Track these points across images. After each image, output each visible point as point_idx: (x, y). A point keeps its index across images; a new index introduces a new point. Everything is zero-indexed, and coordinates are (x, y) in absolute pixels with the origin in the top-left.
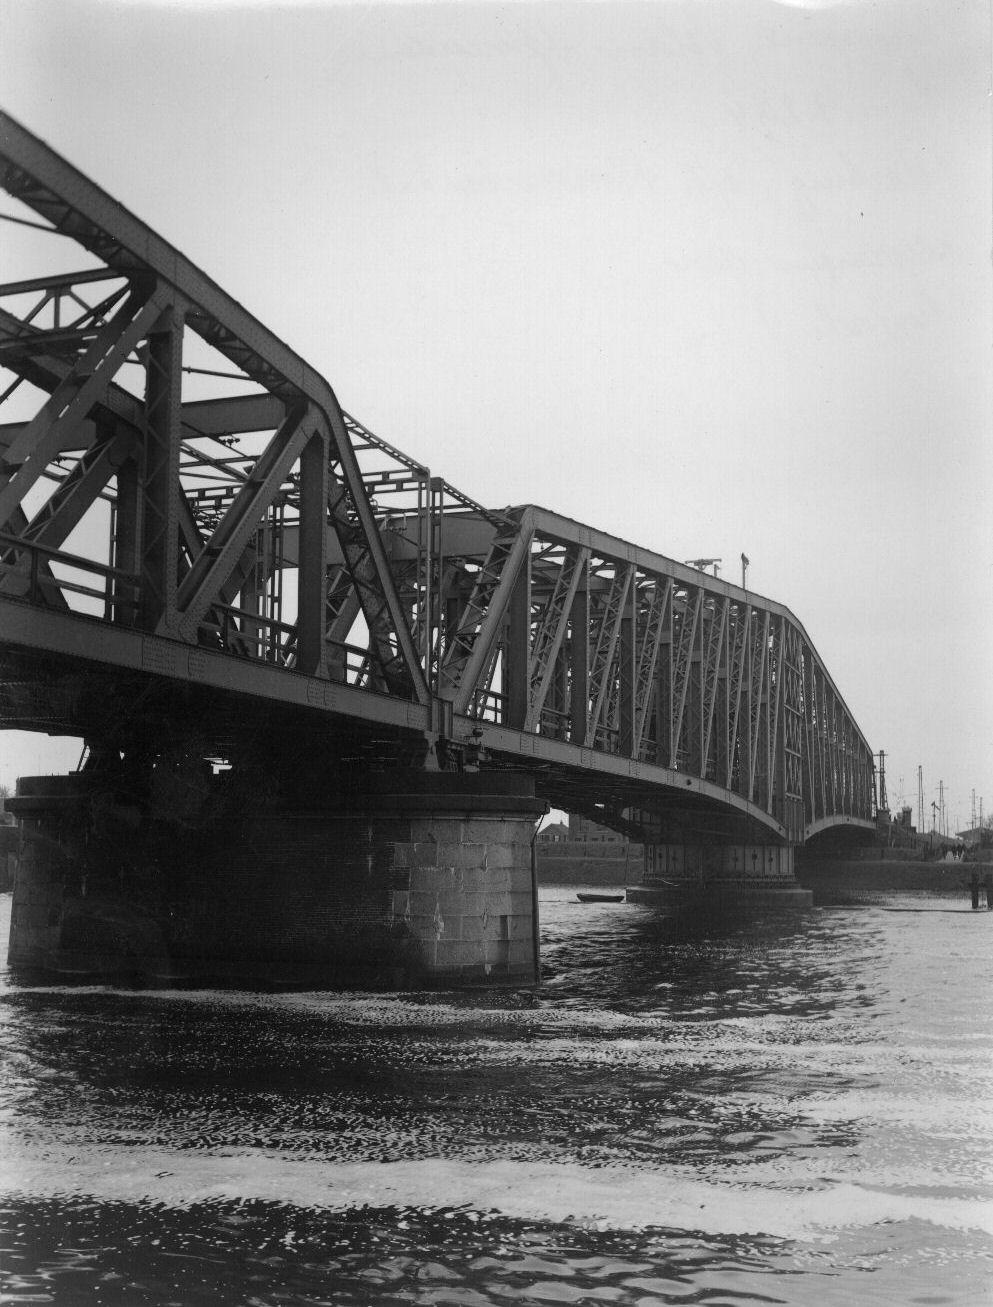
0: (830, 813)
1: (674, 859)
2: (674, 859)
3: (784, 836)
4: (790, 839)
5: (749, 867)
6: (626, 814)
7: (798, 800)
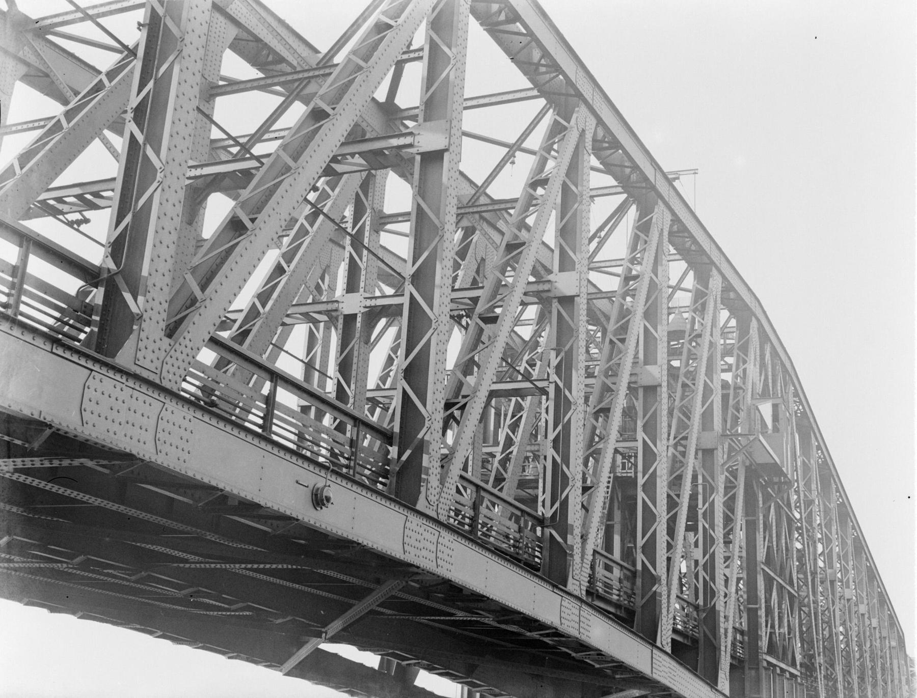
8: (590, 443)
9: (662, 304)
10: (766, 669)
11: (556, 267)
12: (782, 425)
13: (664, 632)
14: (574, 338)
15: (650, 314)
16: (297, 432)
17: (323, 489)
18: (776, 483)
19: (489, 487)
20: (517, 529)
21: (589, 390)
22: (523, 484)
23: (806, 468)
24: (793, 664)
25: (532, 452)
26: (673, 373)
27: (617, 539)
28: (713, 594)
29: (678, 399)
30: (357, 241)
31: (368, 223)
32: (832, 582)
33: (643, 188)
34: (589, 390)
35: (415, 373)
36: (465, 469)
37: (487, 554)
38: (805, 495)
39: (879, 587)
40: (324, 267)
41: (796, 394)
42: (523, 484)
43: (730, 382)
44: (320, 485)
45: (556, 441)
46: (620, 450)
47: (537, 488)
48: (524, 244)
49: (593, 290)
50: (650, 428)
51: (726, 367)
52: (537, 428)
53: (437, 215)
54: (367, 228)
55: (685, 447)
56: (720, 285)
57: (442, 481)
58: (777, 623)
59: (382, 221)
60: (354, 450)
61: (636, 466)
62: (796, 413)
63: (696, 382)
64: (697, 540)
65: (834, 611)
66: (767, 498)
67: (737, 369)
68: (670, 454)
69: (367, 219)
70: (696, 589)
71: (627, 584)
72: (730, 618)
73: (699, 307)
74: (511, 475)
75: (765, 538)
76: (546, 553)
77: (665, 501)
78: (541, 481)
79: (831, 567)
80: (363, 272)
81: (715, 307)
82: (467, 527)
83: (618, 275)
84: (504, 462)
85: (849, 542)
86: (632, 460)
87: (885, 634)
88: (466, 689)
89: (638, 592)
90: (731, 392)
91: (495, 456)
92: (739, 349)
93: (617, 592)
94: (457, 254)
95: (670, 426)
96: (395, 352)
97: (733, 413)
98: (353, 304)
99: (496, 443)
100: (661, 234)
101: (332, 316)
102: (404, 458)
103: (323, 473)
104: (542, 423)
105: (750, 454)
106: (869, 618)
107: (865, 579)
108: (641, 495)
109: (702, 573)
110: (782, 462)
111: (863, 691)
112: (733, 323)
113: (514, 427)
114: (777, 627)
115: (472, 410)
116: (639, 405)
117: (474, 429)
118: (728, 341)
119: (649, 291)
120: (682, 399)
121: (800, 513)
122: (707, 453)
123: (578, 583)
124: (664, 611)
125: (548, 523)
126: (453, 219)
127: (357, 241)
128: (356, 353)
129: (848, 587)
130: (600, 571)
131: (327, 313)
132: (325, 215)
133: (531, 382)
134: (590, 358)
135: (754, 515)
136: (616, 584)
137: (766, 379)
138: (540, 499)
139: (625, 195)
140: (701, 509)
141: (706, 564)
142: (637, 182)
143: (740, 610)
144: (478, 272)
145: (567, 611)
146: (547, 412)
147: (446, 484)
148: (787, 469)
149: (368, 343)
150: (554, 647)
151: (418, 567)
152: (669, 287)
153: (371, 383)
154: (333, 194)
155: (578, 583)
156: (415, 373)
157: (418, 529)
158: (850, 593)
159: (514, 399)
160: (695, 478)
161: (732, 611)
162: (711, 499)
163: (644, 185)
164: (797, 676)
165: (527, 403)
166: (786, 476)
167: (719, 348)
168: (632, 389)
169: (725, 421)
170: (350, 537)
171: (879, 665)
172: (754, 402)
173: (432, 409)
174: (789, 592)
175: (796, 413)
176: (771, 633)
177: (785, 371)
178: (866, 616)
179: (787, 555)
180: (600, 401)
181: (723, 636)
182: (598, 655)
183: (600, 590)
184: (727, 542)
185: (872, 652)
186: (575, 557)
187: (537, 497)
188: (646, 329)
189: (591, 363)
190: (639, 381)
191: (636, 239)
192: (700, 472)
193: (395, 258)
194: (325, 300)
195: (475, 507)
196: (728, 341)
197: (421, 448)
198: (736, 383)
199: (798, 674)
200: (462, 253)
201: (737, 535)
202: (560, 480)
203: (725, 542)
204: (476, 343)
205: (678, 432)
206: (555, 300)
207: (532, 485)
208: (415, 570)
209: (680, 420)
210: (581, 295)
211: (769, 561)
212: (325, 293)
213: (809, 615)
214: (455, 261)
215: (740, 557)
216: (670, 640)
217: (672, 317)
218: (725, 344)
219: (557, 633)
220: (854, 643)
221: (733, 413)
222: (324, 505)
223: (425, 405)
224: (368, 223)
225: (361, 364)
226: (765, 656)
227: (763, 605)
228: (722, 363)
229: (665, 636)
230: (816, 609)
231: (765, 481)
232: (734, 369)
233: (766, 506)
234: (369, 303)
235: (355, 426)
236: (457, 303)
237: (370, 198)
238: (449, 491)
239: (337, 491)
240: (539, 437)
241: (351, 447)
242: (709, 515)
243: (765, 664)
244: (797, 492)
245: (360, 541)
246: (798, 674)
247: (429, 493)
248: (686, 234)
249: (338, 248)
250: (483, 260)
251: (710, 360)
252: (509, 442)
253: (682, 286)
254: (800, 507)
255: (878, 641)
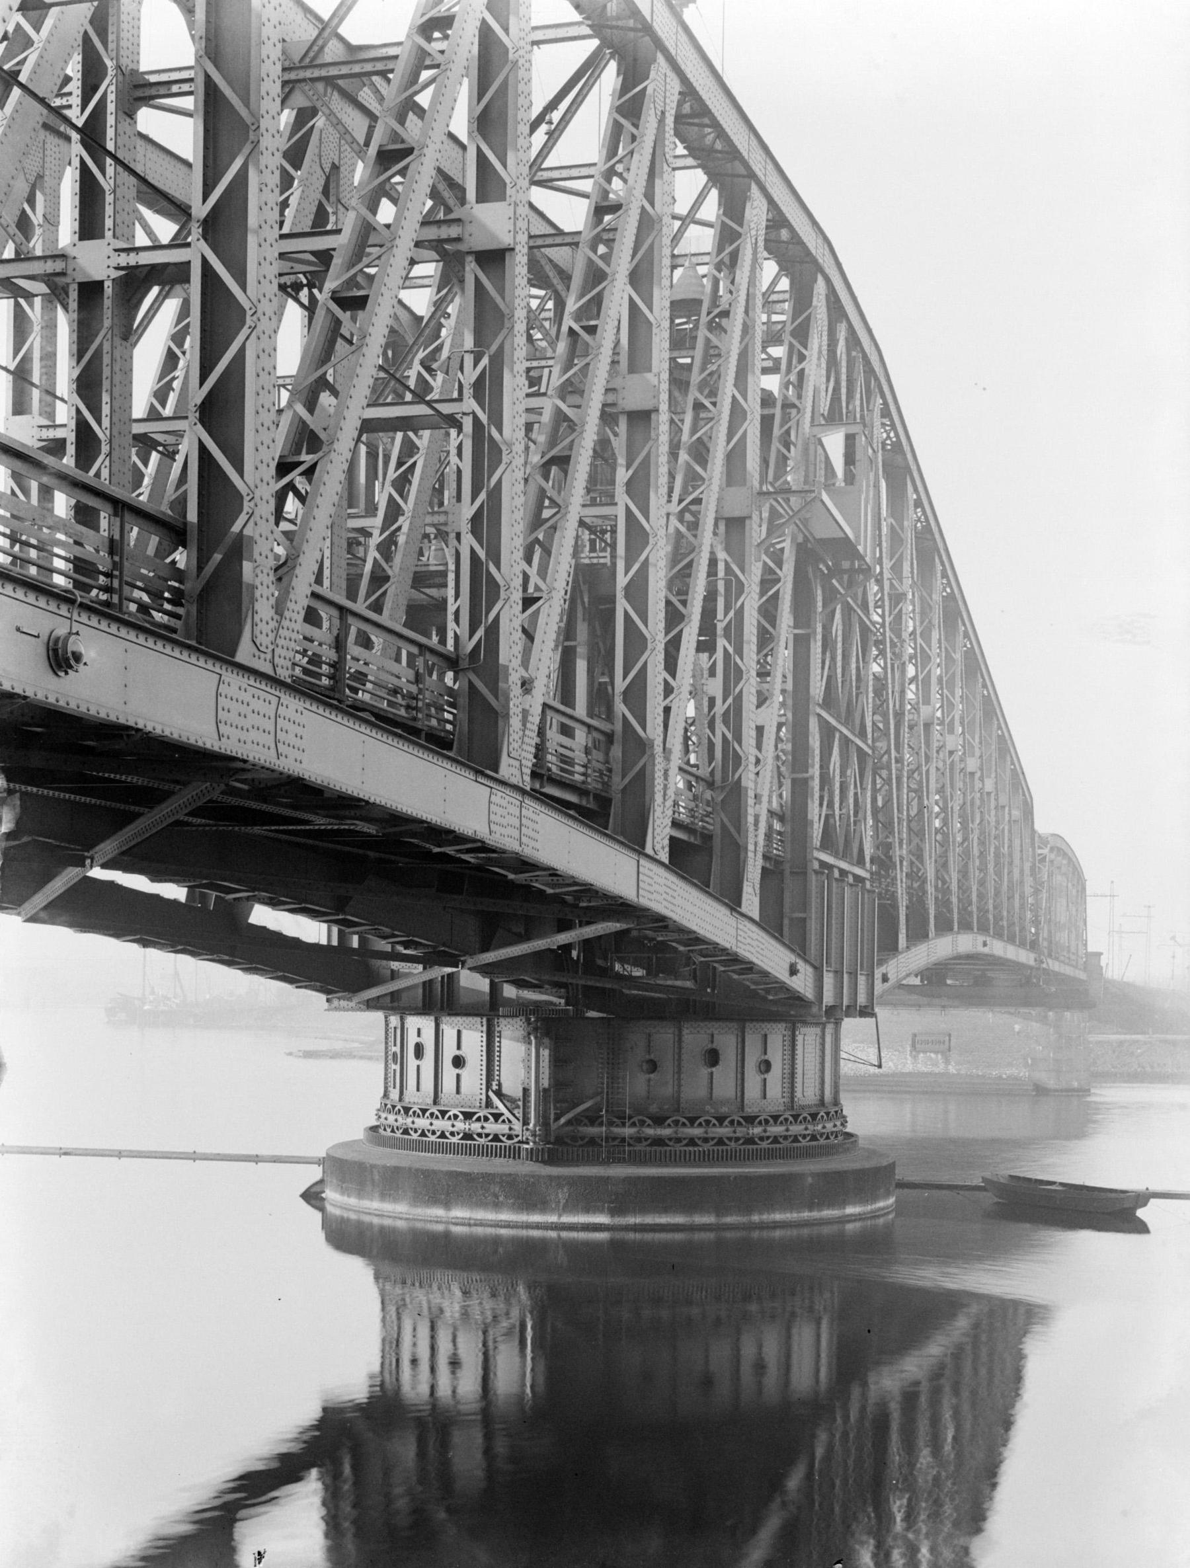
0: (945, 927)
1: (458, 1062)
2: (458, 1062)
3: (809, 994)
4: (828, 998)
5: (694, 1089)
6: (937, 823)
7: (858, 879)
8: (536, 522)
9: (657, 466)
10: (816, 872)
11: (471, 194)
12: (859, 469)
13: (658, 830)
14: (505, 331)
15: (641, 277)
16: (8, 531)
17: (67, 639)
18: (845, 571)
19: (360, 606)
20: (412, 678)
21: (533, 418)
22: (421, 579)
23: (896, 538)
24: (860, 862)
25: (434, 525)
26: (679, 379)
27: (581, 666)
28: (738, 760)
29: (686, 427)
30: (92, 135)
31: (111, 97)
32: (927, 726)
33: (631, 29)
34: (533, 418)
35: (220, 410)
36: (319, 580)
37: (363, 729)
38: (892, 584)
39: (1000, 728)
40: (32, 179)
41: (886, 413)
42: (421, 579)
43: (776, 394)
44: (61, 631)
45: (476, 520)
46: (587, 520)
47: (445, 585)
48: (410, 151)
49: (540, 228)
50: (639, 488)
51: (769, 364)
52: (441, 480)
53: (247, 103)
54: (111, 107)
55: (695, 514)
56: (764, 218)
57: (279, 609)
58: (837, 799)
59: (142, 91)
60: (117, 559)
61: (613, 546)
62: (884, 444)
63: (718, 399)
64: (714, 663)
65: (928, 771)
66: (831, 596)
67: (789, 371)
68: (671, 530)
69: (109, 88)
70: (711, 745)
71: (597, 755)
72: (763, 792)
73: (727, 260)
74: (399, 568)
75: (823, 662)
76: (464, 717)
77: (662, 615)
78: (451, 577)
79: (927, 702)
80: (109, 198)
81: (755, 260)
82: (325, 681)
83: (585, 196)
84: (387, 548)
85: (958, 656)
86: (608, 536)
87: (1003, 800)
88: (335, 929)
89: (617, 767)
90: (778, 411)
91: (370, 535)
92: (794, 334)
93: (582, 770)
94: (286, 155)
95: (672, 476)
96: (180, 345)
97: (779, 451)
98: (98, 261)
99: (371, 510)
100: (661, 121)
101: (57, 291)
102: (210, 568)
103: (64, 610)
104: (450, 471)
105: (805, 522)
106: (982, 779)
107: (979, 714)
108: (622, 605)
109: (720, 727)
110: (858, 537)
111: (964, 892)
112: (784, 284)
113: (402, 484)
114: (837, 805)
115: (326, 478)
116: (619, 444)
117: (332, 510)
118: (775, 318)
119: (638, 236)
120: (694, 430)
121: (883, 616)
122: (734, 526)
123: (517, 763)
124: (658, 798)
125: (464, 664)
126: (276, 89)
127: (92, 135)
128: (106, 359)
129: (951, 731)
130: (553, 735)
131: (48, 279)
132: (22, 86)
133: (429, 404)
134: (535, 354)
135: (809, 626)
136: (579, 757)
137: (837, 390)
138: (451, 609)
139: (595, 43)
140: (722, 620)
141: (727, 712)
142: (618, 18)
143: (780, 774)
144: (326, 192)
145: (500, 811)
146: (460, 454)
147: (286, 614)
148: (865, 548)
149: (129, 334)
150: (478, 868)
151: (245, 761)
152: (674, 217)
153: (139, 409)
154: (39, 38)
155: (517, 763)
156: (220, 410)
157: (243, 696)
158: (952, 742)
159: (399, 435)
160: (713, 562)
161: (767, 786)
162: (737, 690)
163: (631, 23)
164: (864, 879)
165: (424, 439)
166: (861, 558)
167: (759, 332)
168: (608, 416)
169: (765, 461)
170: (122, 721)
171: (992, 850)
172: (816, 430)
173: (255, 477)
174: (859, 749)
175: (884, 444)
176: (827, 816)
177: (869, 371)
178: (978, 775)
179: (858, 688)
180: (553, 442)
181: (751, 828)
182: (551, 875)
183: (554, 769)
184: (763, 674)
185: (982, 832)
186: (512, 721)
187: (445, 601)
188: (632, 304)
189: (535, 364)
190: (620, 402)
191: (616, 131)
192: (722, 555)
193: (168, 158)
194: (39, 253)
195: (339, 644)
196: (775, 318)
197: (239, 549)
198: (786, 397)
199: (867, 875)
200: (295, 155)
201: (780, 656)
202: (484, 592)
203: (759, 675)
204: (327, 345)
205: (685, 492)
206: (470, 258)
207: (438, 580)
208: (241, 765)
209: (690, 471)
210: (518, 248)
211: (829, 701)
212: (38, 231)
213: (888, 781)
214: (284, 171)
215: (783, 691)
216: (666, 842)
217: (678, 272)
218: (769, 323)
219: (482, 847)
220: (956, 816)
221: (779, 451)
222: (71, 667)
223: (241, 472)
224: (111, 97)
225: (117, 379)
226: (816, 854)
227: (817, 773)
228: (764, 356)
229: (659, 835)
230: (900, 770)
231: (828, 567)
232: (783, 367)
233: (829, 610)
234: (124, 260)
235: (116, 515)
236: (290, 260)
237: (111, 46)
238: (292, 625)
239: (97, 646)
240: (446, 493)
241: (111, 552)
242: (735, 632)
243: (816, 865)
244: (879, 582)
245: (140, 726)
246: (867, 875)
247: (257, 632)
248: (706, 121)
249: (56, 141)
250: (335, 168)
251: (744, 356)
252: (394, 511)
253: (698, 216)
254: (882, 607)
255: (993, 813)
